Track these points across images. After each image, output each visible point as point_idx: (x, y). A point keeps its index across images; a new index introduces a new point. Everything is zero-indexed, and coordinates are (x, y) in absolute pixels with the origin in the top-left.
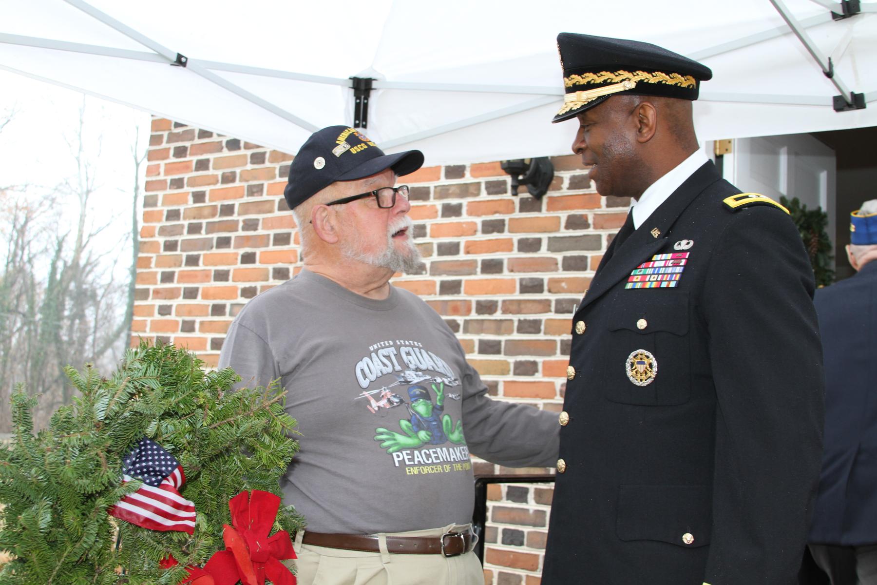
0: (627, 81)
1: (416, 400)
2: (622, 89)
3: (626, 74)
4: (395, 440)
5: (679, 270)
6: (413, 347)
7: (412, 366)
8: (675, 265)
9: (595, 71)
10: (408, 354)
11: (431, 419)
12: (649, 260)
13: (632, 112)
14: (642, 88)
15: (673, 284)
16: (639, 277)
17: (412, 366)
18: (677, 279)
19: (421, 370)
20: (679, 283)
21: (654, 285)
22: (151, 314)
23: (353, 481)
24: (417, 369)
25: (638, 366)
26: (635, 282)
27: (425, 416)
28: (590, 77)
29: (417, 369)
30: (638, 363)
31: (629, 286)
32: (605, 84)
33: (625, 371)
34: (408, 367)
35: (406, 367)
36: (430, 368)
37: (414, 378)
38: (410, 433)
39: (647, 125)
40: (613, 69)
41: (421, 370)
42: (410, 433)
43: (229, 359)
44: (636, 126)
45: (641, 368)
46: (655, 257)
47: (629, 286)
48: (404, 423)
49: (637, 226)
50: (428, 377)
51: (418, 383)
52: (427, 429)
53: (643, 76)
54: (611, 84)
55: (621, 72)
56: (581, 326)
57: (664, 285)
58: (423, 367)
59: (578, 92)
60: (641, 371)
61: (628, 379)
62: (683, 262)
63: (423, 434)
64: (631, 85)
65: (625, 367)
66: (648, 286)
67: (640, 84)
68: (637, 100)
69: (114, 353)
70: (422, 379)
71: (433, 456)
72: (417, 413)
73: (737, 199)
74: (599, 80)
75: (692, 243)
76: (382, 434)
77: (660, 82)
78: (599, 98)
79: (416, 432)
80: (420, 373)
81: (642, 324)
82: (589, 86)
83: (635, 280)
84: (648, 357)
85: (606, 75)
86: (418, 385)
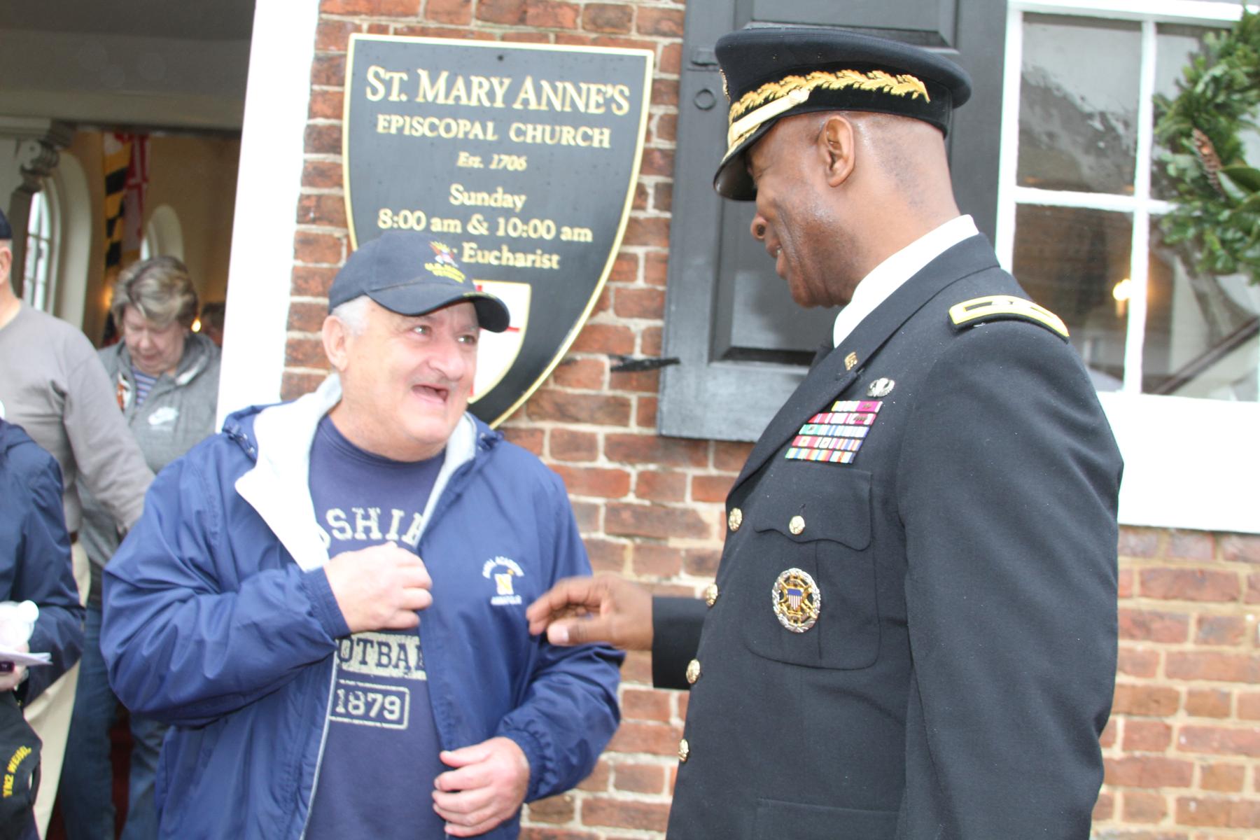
3: (793, 81)
5: (861, 432)
8: (859, 423)
12: (827, 409)
13: (816, 140)
14: (821, 101)
15: (846, 458)
16: (808, 439)
18: (855, 448)
21: (822, 456)
22: (1184, 781)
30: (791, 592)
31: (791, 453)
33: (772, 605)
39: (840, 157)
40: (777, 77)
43: (488, 811)
44: (825, 162)
45: (795, 601)
46: (839, 406)
49: (836, 344)
53: (822, 79)
56: (737, 515)
57: (834, 459)
61: (775, 616)
62: (870, 419)
64: (802, 96)
65: (771, 598)
69: (785, 253)
73: (968, 309)
75: (892, 384)
78: (763, 124)
81: (797, 524)
83: (801, 444)
85: (768, 89)
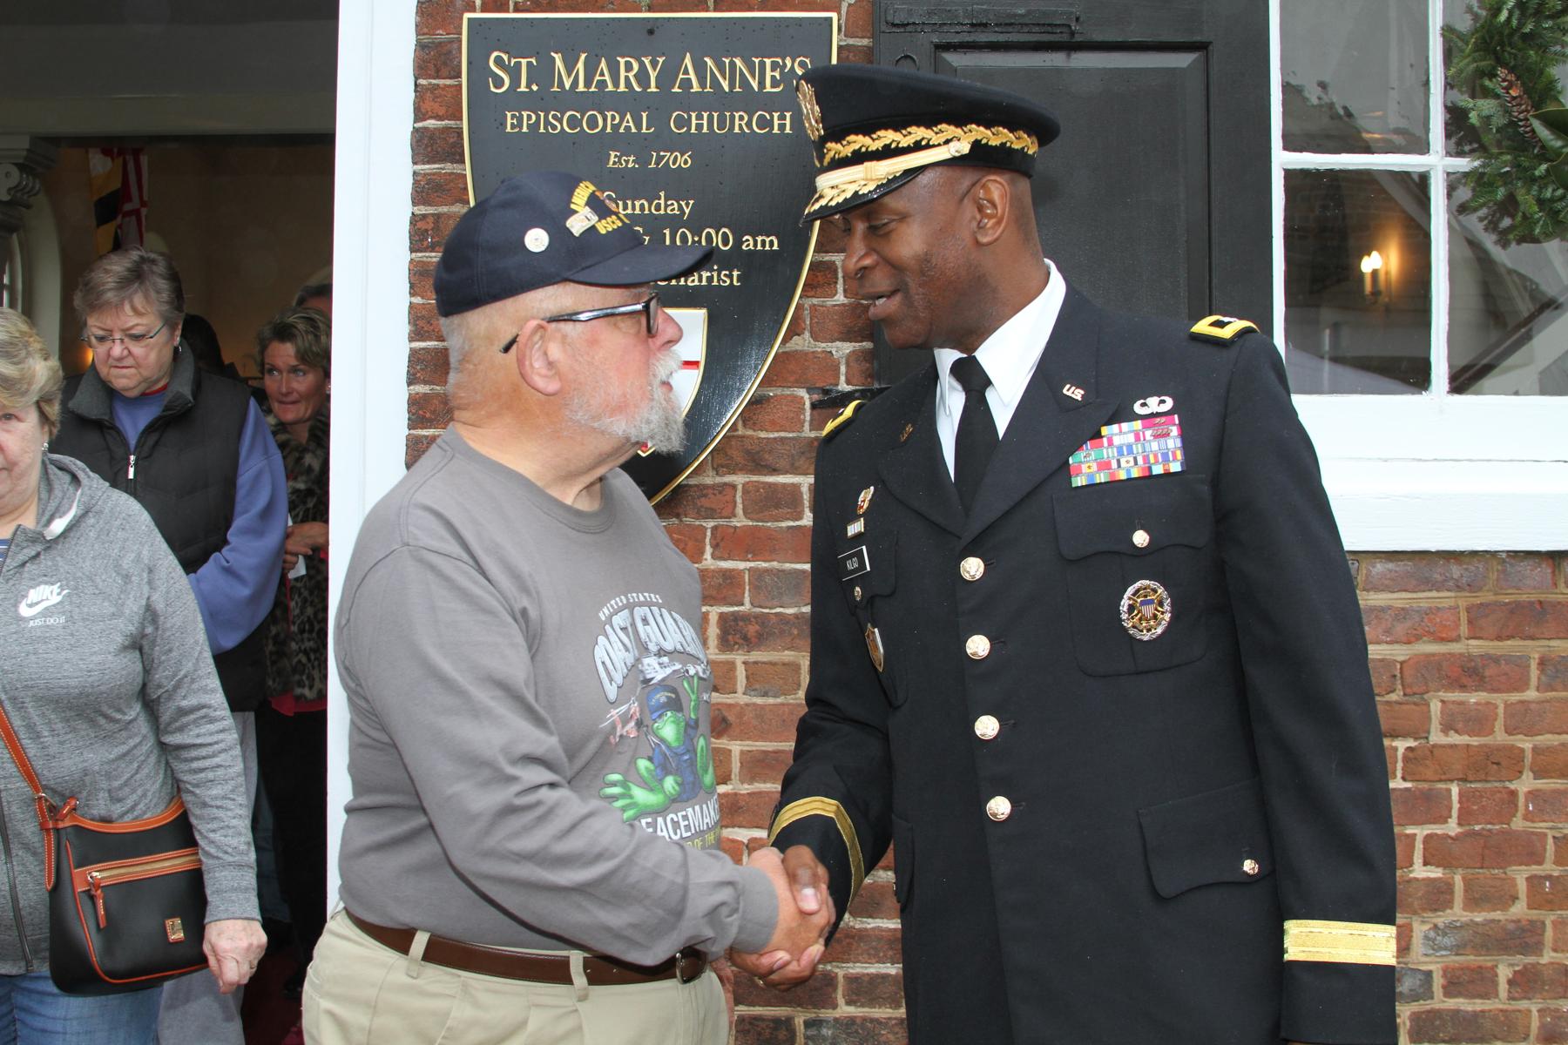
0: (955, 142)
1: (660, 716)
2: (948, 156)
3: (949, 130)
4: (631, 797)
6: (649, 604)
7: (653, 648)
9: (868, 131)
10: (645, 621)
11: (680, 751)
14: (981, 157)
15: (1176, 467)
17: (653, 648)
19: (667, 653)
20: (1187, 462)
23: (218, 847)
24: (661, 652)
25: (1143, 608)
26: (1087, 467)
27: (674, 744)
28: (888, 137)
29: (661, 652)
30: (1143, 603)
32: (918, 147)
34: (647, 649)
35: (643, 649)
36: (679, 647)
37: (656, 670)
38: (654, 784)
41: (667, 653)
42: (654, 784)
47: (1079, 481)
48: (643, 764)
50: (678, 666)
51: (663, 680)
52: (677, 772)
54: (928, 146)
55: (943, 126)
58: (668, 646)
59: (867, 164)
60: (1149, 615)
62: (1174, 431)
63: (670, 783)
64: (963, 147)
66: (1123, 476)
67: (976, 145)
68: (966, 179)
70: (669, 671)
71: (683, 824)
72: (663, 740)
74: (904, 143)
76: (614, 784)
77: (1003, 144)
79: (661, 781)
80: (665, 659)
82: (888, 152)
84: (1155, 591)
85: (918, 133)
86: (664, 685)
